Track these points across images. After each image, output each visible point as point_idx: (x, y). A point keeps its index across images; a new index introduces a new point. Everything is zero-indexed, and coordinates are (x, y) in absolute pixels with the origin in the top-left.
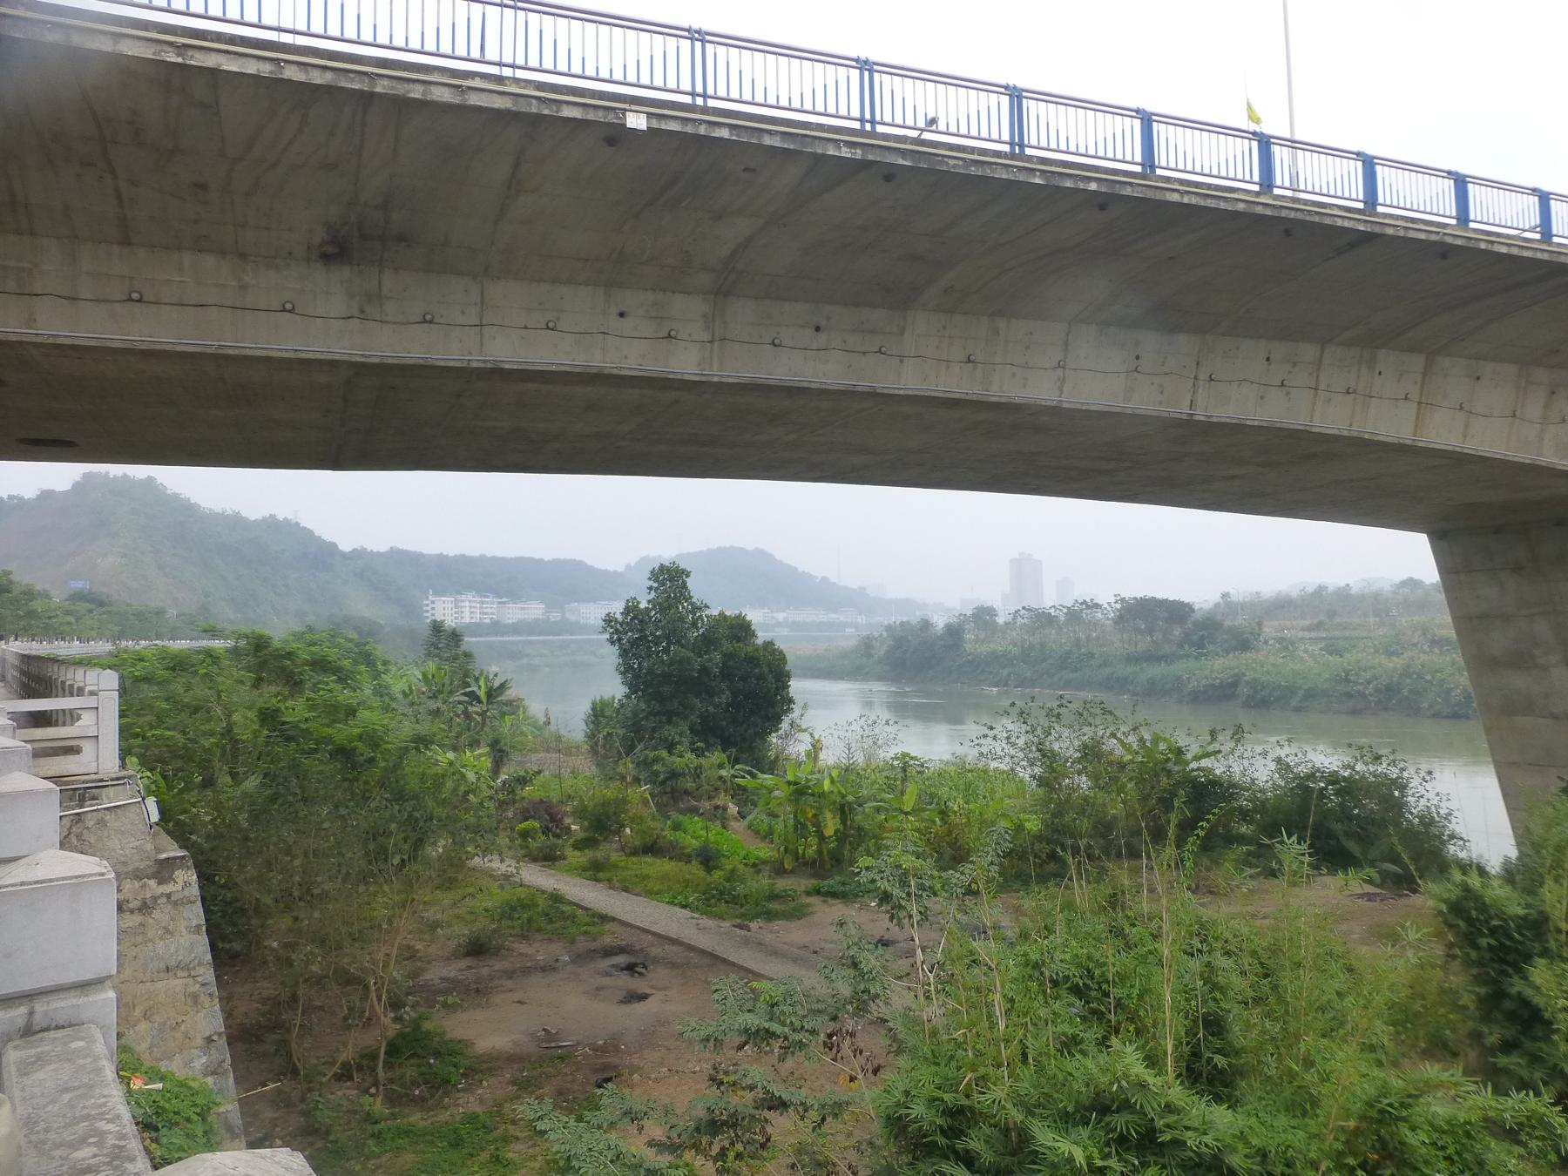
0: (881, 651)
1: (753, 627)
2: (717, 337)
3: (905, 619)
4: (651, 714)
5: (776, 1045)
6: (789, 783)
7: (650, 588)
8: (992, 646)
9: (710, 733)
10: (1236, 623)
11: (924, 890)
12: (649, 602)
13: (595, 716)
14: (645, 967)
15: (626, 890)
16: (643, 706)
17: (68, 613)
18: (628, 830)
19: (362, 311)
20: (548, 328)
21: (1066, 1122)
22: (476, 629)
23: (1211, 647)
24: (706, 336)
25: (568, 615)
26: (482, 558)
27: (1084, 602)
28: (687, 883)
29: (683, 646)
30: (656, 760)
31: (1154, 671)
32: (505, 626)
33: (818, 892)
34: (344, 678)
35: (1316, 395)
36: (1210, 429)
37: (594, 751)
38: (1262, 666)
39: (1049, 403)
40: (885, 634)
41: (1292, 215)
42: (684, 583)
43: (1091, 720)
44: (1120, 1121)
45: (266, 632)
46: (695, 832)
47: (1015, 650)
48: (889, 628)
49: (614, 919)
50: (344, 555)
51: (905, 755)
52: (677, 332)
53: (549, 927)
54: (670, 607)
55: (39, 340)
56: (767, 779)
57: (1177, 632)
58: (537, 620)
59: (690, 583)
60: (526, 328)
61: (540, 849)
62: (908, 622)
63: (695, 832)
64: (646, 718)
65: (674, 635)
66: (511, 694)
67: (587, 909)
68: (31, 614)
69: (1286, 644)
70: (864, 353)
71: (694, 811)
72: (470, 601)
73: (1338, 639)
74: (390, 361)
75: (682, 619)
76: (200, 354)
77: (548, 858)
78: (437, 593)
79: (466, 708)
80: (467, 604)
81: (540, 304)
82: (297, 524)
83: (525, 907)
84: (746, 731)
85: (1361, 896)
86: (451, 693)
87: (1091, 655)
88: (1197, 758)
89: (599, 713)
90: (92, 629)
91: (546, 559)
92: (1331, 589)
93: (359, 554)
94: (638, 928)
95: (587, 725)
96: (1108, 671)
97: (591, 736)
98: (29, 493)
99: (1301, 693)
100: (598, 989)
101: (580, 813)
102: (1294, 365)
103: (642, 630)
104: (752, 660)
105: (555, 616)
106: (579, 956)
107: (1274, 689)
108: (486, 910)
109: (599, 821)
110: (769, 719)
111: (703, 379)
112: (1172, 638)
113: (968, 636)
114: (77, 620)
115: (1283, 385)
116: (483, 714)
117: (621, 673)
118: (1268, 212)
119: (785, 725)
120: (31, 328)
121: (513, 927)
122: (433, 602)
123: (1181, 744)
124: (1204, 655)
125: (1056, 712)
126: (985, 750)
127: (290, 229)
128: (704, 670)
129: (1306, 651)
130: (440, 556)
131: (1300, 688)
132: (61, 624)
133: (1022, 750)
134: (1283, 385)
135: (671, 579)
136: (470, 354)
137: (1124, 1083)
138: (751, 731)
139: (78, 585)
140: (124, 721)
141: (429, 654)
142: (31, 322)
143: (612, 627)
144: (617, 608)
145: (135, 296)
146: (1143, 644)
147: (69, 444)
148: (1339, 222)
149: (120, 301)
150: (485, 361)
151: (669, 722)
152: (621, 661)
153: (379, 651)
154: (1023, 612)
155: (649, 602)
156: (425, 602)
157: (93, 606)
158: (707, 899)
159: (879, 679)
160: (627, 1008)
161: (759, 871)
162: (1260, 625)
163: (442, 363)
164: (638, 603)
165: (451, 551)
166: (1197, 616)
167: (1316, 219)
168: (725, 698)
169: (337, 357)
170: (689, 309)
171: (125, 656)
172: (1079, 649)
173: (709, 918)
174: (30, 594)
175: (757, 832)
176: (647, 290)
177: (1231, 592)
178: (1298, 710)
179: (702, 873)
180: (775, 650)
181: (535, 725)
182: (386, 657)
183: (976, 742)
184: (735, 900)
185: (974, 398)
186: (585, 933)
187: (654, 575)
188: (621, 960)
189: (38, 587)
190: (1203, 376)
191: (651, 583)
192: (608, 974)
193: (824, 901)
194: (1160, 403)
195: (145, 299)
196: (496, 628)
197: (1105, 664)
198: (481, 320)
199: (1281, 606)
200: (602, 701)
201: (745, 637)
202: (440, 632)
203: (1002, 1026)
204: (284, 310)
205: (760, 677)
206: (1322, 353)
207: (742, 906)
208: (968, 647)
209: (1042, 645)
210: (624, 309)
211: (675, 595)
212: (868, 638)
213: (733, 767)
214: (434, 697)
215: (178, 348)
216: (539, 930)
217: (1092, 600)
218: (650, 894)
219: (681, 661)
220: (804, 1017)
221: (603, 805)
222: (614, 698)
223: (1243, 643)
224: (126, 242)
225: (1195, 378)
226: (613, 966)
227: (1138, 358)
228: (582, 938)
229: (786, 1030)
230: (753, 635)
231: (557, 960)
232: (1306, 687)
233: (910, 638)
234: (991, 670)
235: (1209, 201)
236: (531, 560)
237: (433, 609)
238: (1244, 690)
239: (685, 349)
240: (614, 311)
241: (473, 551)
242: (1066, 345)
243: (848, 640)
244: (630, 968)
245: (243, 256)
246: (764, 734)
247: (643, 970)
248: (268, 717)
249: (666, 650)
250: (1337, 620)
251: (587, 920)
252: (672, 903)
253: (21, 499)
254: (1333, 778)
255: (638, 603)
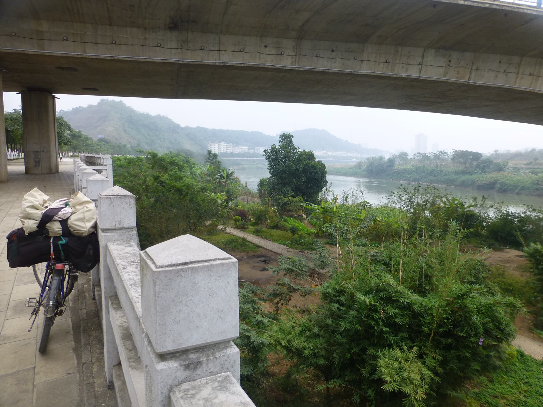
0: (364, 167)
1: (314, 156)
2: (297, 54)
3: (374, 156)
4: (278, 184)
5: (294, 274)
6: (322, 208)
7: (280, 141)
8: (405, 166)
9: (297, 191)
10: (498, 161)
11: (343, 234)
12: (279, 146)
13: (261, 184)
14: (269, 261)
15: (266, 239)
16: (276, 181)
17: (98, 145)
18: (269, 221)
19: (182, 46)
20: (241, 51)
21: (367, 293)
22: (224, 155)
23: (487, 170)
24: (294, 54)
25: (256, 151)
26: (228, 130)
27: (441, 152)
28: (286, 238)
29: (290, 161)
30: (280, 199)
31: (465, 178)
32: (235, 154)
33: (329, 243)
34: (181, 168)
35: (517, 76)
36: (476, 87)
37: (260, 196)
38: (506, 177)
39: (415, 77)
40: (366, 161)
41: (507, 8)
42: (291, 140)
43: (430, 191)
44: (381, 294)
45: (156, 152)
46: (291, 223)
47: (413, 168)
48: (368, 159)
49: (261, 247)
50: (182, 128)
51: (365, 202)
52: (284, 52)
53: (241, 248)
54: (286, 148)
55: (87, 57)
56: (315, 206)
57: (475, 164)
58: (245, 152)
59: (293, 140)
60: (234, 51)
61: (240, 225)
62: (375, 157)
63: (291, 223)
64: (277, 185)
65: (287, 157)
66: (234, 176)
67: (253, 244)
68: (87, 145)
69: (517, 169)
70: (349, 59)
71: (292, 216)
72: (223, 145)
73: (537, 168)
74: (190, 63)
75: (290, 152)
76: (133, 61)
77: (243, 228)
78: (212, 142)
79: (220, 180)
80: (222, 146)
81: (238, 43)
82: (167, 118)
83: (234, 242)
84: (310, 191)
85: (519, 256)
86: (214, 175)
87: (442, 171)
88: (469, 207)
89: (262, 183)
90: (105, 151)
91: (249, 131)
92: (537, 150)
93: (187, 128)
94: (269, 250)
95: (258, 187)
96: (447, 177)
97: (259, 191)
98: (85, 106)
99: (519, 188)
100: (254, 266)
101: (254, 215)
102: (510, 64)
103: (276, 156)
104: (314, 167)
105: (252, 151)
106: (249, 257)
107: (509, 186)
108: (222, 242)
109: (259, 217)
110: (318, 187)
111: (292, 69)
112: (473, 166)
113: (397, 163)
114: (101, 147)
115: (505, 72)
116: (225, 182)
117: (269, 170)
118: (498, 8)
119: (324, 189)
120: (85, 53)
121: (230, 248)
122: (211, 145)
123: (463, 201)
124: (484, 172)
125: (417, 188)
126: (391, 200)
127: (159, 19)
128: (297, 170)
129: (523, 173)
130: (214, 129)
131: (519, 186)
132: (96, 149)
133: (404, 201)
134: (505, 72)
135: (287, 138)
136: (216, 60)
137: (384, 283)
138: (312, 191)
139: (100, 136)
140: (115, 178)
141: (207, 161)
142: (85, 51)
143: (266, 154)
144: (268, 148)
145: (114, 42)
146: (462, 167)
147: (97, 90)
148: (526, 11)
149: (109, 44)
150: (220, 63)
151: (285, 187)
152: (269, 165)
153: (192, 161)
154: (417, 154)
155: (279, 146)
156: (208, 145)
157: (105, 143)
158: (292, 243)
159: (363, 177)
160: (262, 272)
161: (310, 236)
162: (507, 162)
163: (207, 64)
164: (276, 146)
165: (217, 128)
166: (483, 158)
167: (517, 10)
168: (304, 179)
169: (174, 62)
170: (288, 44)
171: (115, 159)
172: (437, 169)
173: (292, 249)
174: (87, 139)
175: (312, 224)
176: (274, 38)
177: (498, 149)
178: (517, 194)
179: (291, 235)
180: (322, 164)
181: (242, 187)
182: (194, 162)
183: (388, 197)
184: (301, 244)
185: (388, 75)
186: (252, 250)
187: (281, 137)
188: (262, 259)
189: (89, 137)
190: (474, 68)
191: (280, 139)
192: (258, 263)
193: (330, 246)
194: (457, 78)
195: (116, 43)
196: (232, 154)
197: (445, 175)
198: (219, 49)
199: (518, 155)
200: (263, 179)
201: (312, 159)
202: (210, 154)
203: (354, 268)
204: (158, 46)
205: (316, 173)
206: (521, 60)
207: (303, 246)
208: (396, 167)
209: (424, 167)
210: (266, 45)
211: (288, 144)
212: (360, 162)
213: (305, 203)
214: (209, 176)
215: (127, 59)
216: (238, 249)
217: (444, 151)
218: (274, 240)
219: (289, 166)
220: (303, 267)
221: (261, 212)
222: (267, 178)
223: (500, 168)
224: (111, 25)
225: (471, 69)
226: (260, 260)
227: (450, 61)
228: (251, 252)
229: (297, 270)
230: (315, 158)
231: (243, 258)
232: (521, 186)
233: (375, 163)
234: (404, 175)
235: (475, 4)
236: (244, 131)
237: (211, 147)
238: (498, 186)
239: (287, 58)
240: (263, 45)
241: (225, 128)
242: (423, 56)
243: (353, 163)
244: (265, 261)
245: (145, 28)
246: (316, 192)
247: (269, 262)
248: (156, 178)
249: (285, 162)
250: (538, 162)
251: (253, 247)
252: (281, 244)
253: (83, 108)
254: (519, 217)
255: (276, 146)
